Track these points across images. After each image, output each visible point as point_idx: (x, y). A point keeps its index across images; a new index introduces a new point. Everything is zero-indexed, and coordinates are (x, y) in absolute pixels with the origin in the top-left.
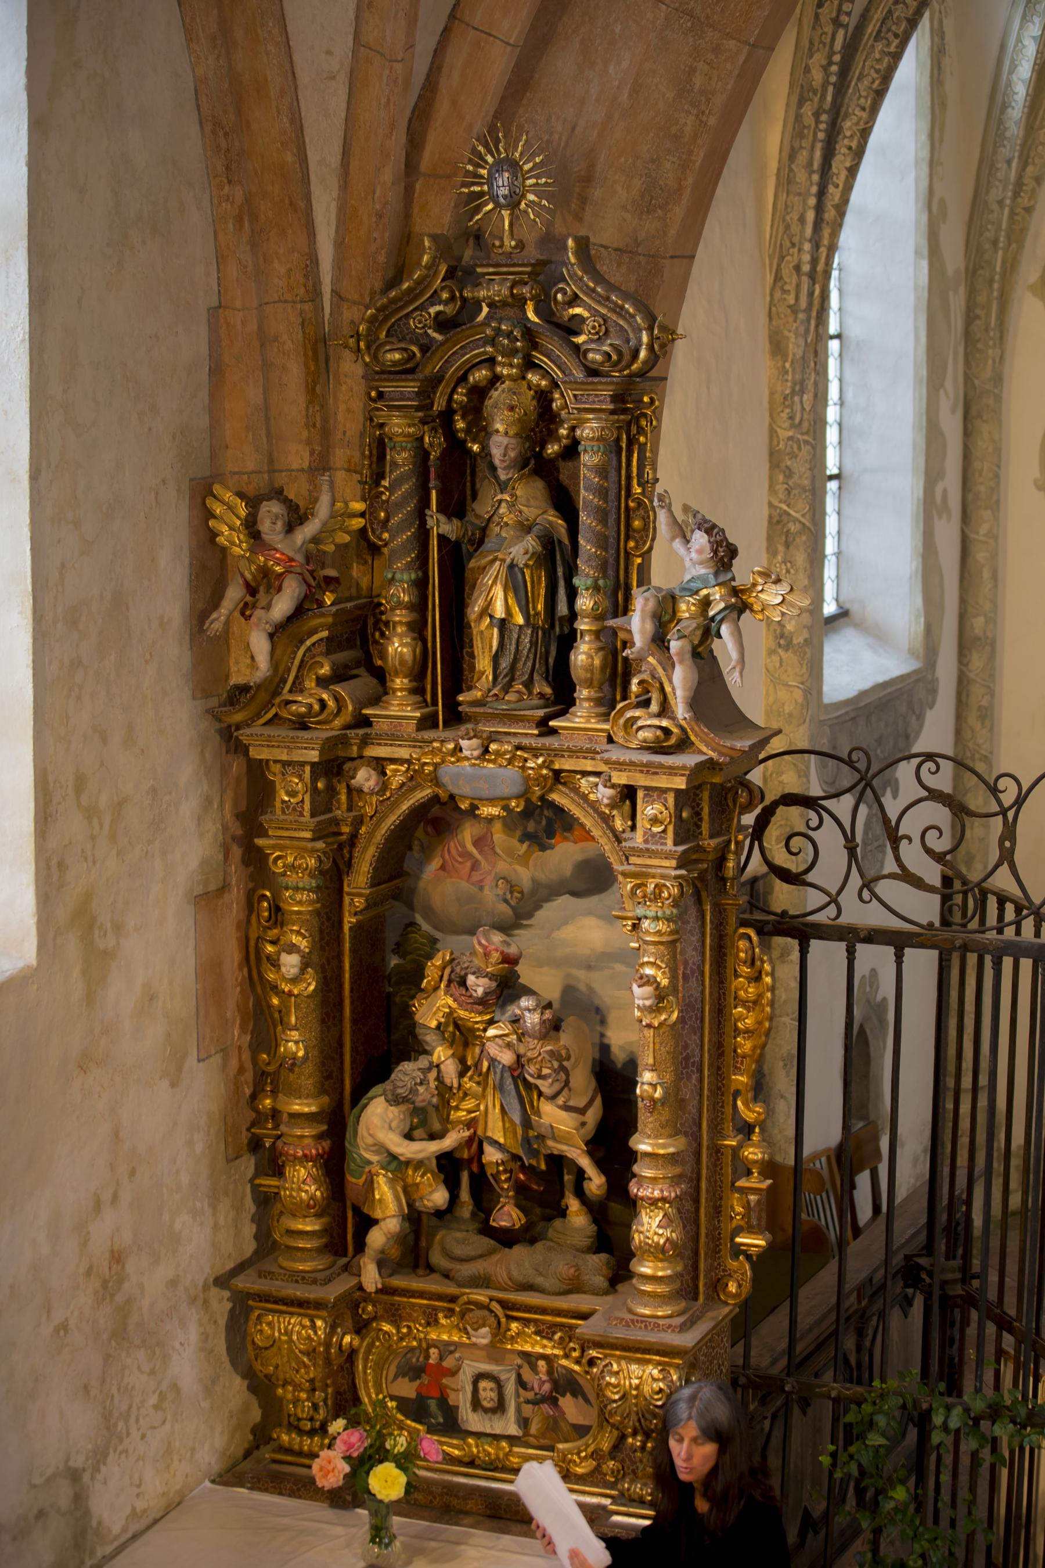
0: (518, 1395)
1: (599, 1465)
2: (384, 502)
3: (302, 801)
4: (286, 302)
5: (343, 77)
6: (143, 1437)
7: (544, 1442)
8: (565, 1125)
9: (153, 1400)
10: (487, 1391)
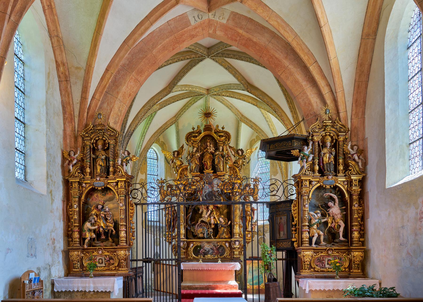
5: (79, 103)
8: (111, 226)
10: (100, 261)
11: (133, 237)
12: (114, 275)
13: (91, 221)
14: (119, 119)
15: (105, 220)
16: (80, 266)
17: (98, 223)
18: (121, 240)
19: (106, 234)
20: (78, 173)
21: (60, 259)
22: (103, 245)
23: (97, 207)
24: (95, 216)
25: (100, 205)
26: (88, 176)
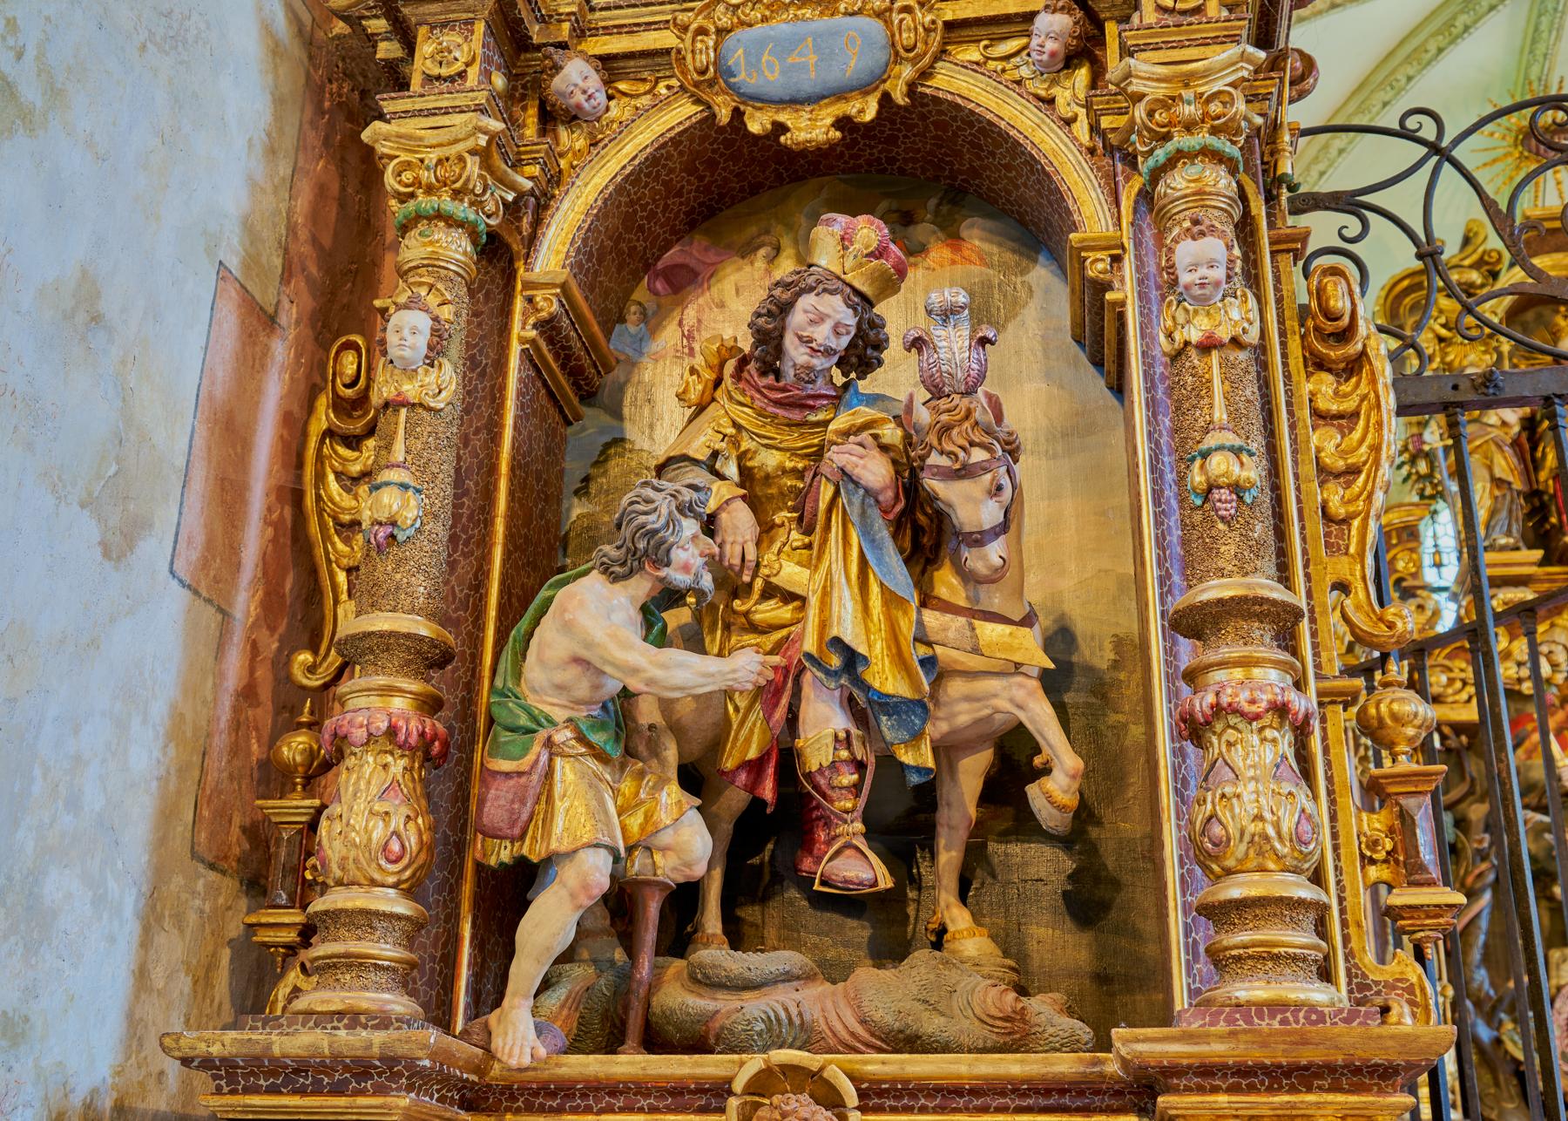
13: (647, 552)
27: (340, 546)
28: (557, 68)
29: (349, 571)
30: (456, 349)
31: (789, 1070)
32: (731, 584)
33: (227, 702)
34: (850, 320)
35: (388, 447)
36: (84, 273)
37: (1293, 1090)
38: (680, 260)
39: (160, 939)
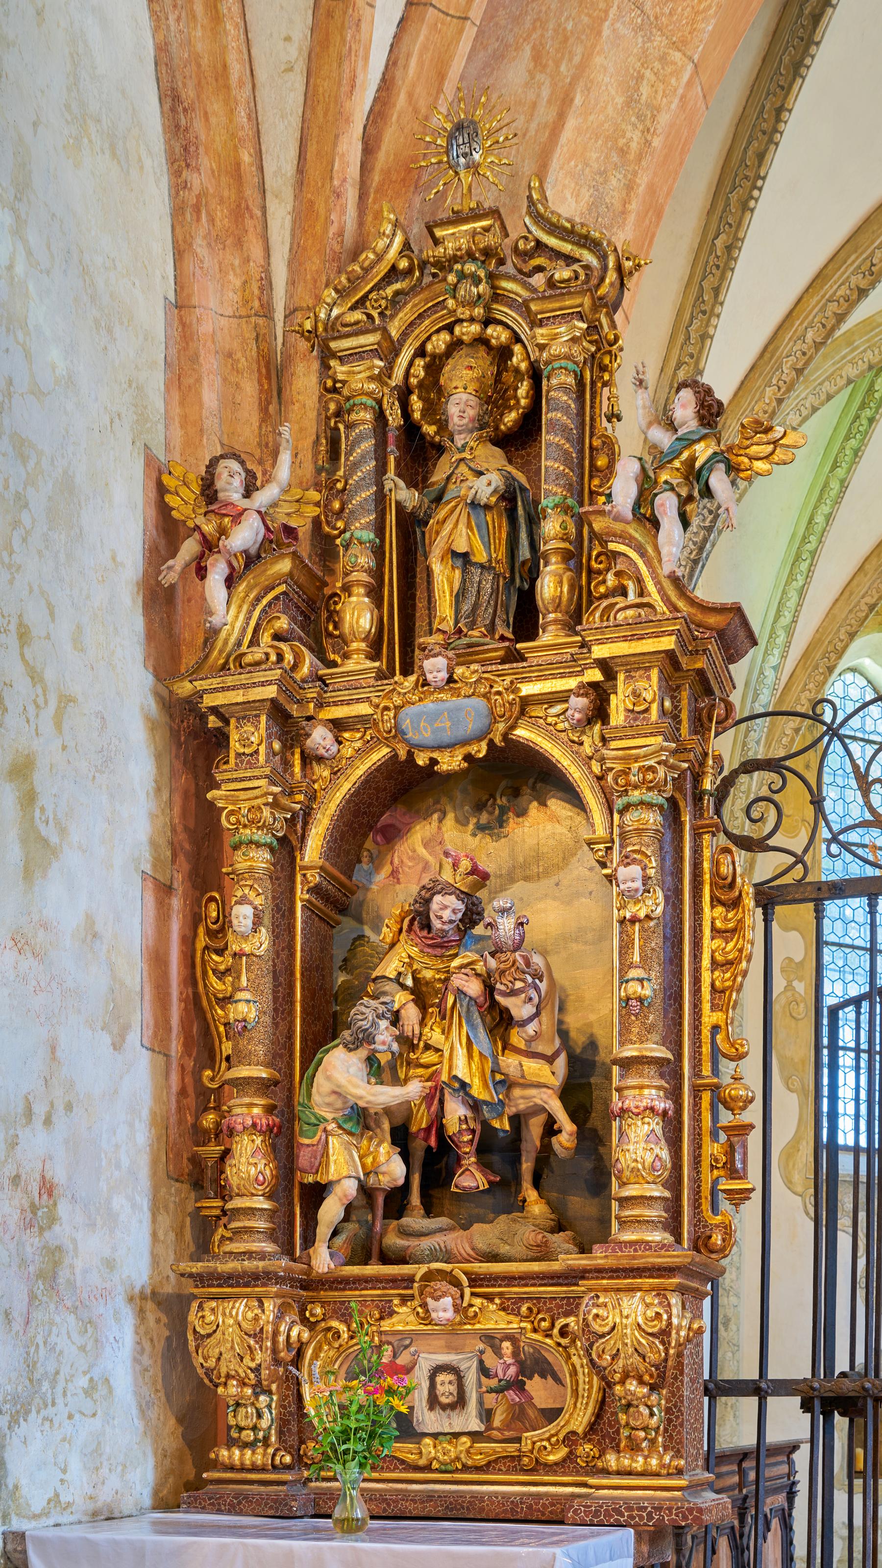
0: (480, 1384)
1: (571, 1452)
2: (339, 491)
3: (257, 752)
4: (240, 317)
5: (301, 67)
6: (70, 1417)
7: (508, 1434)
8: (540, 1082)
9: (83, 1382)
10: (446, 1386)
11: (734, 1174)
12: (551, 1515)
13: (366, 1038)
14: (630, 187)
15: (491, 1032)
16: (283, 1424)
17: (429, 1057)
18: (624, 1202)
19: (499, 1148)
20: (277, 637)
21: (119, 1357)
22: (465, 1248)
23: (419, 918)
24: (401, 998)
25: (446, 889)
26: (358, 662)
27: (219, 1011)
28: (308, 735)
29: (225, 1025)
30: (267, 920)
31: (439, 1271)
32: (408, 1043)
33: (173, 1099)
34: (461, 906)
35: (238, 977)
36: (87, 915)
37: (634, 1277)
38: (389, 822)
39: (160, 1218)
